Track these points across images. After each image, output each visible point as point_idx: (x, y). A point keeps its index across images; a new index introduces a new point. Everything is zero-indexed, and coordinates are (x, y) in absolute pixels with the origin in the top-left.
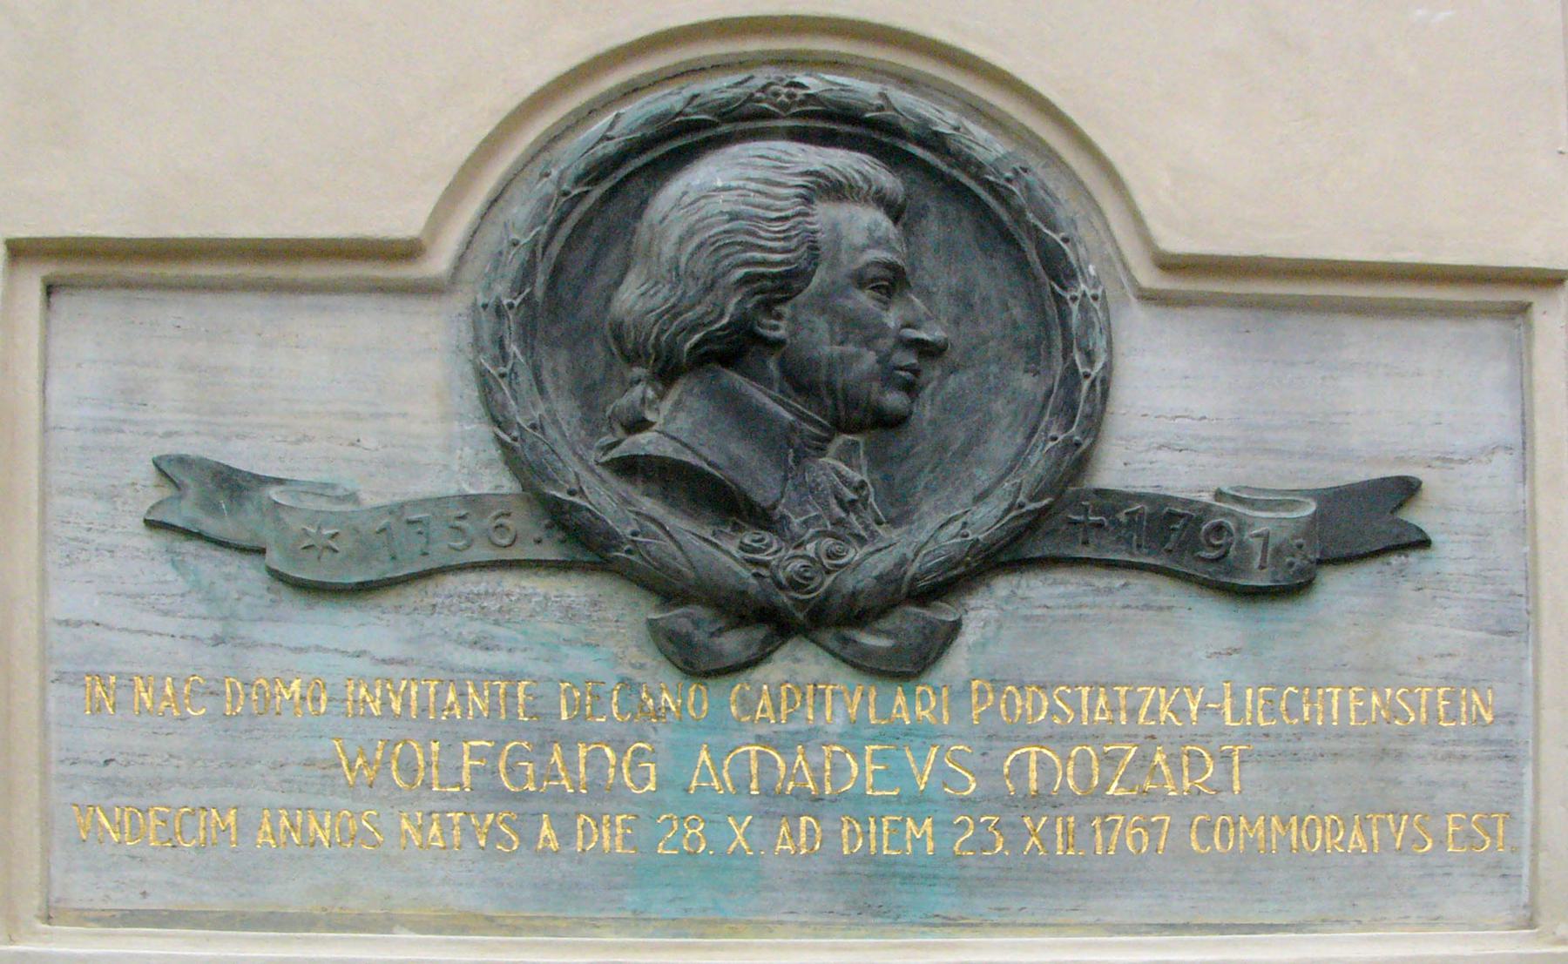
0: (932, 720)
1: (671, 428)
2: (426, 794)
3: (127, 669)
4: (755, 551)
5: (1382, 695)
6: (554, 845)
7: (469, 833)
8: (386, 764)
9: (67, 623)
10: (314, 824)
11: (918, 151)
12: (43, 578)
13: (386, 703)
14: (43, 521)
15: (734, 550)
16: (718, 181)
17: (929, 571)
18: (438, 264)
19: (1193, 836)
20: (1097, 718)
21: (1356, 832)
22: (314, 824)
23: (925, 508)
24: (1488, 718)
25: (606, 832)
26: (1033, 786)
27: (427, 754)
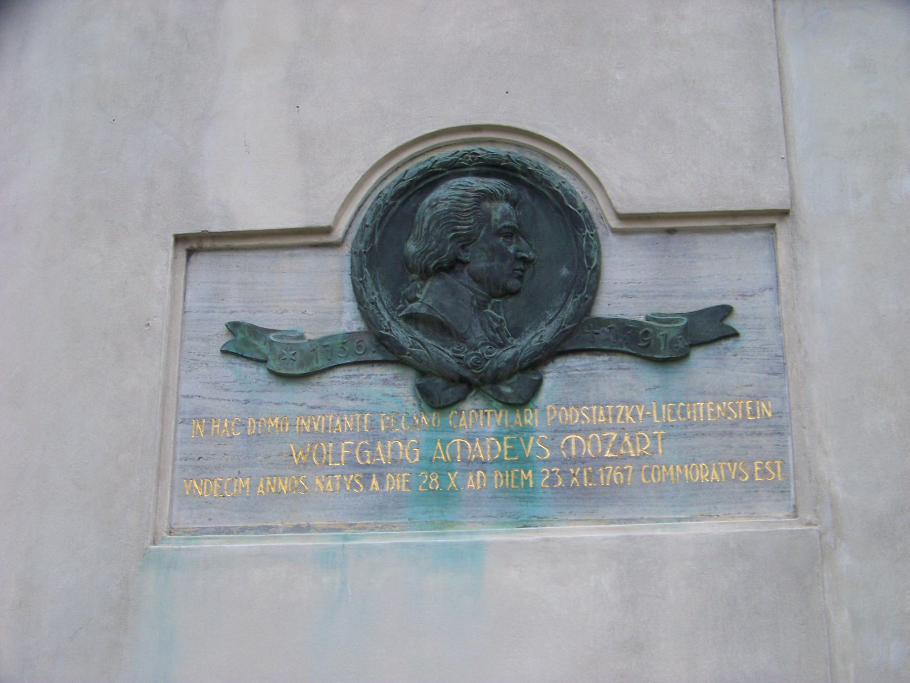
0: (531, 424)
1: (426, 301)
2: (326, 467)
3: (209, 416)
4: (459, 352)
5: (722, 405)
6: (377, 488)
7: (342, 483)
8: (311, 454)
9: (187, 396)
10: (280, 483)
11: (523, 177)
12: (179, 378)
13: (312, 426)
14: (181, 352)
15: (449, 352)
16: (445, 193)
17: (528, 358)
18: (339, 233)
19: (643, 475)
20: (600, 420)
21: (714, 472)
22: (280, 483)
23: (527, 329)
24: (770, 415)
25: (398, 481)
26: (574, 453)
27: (328, 449)
